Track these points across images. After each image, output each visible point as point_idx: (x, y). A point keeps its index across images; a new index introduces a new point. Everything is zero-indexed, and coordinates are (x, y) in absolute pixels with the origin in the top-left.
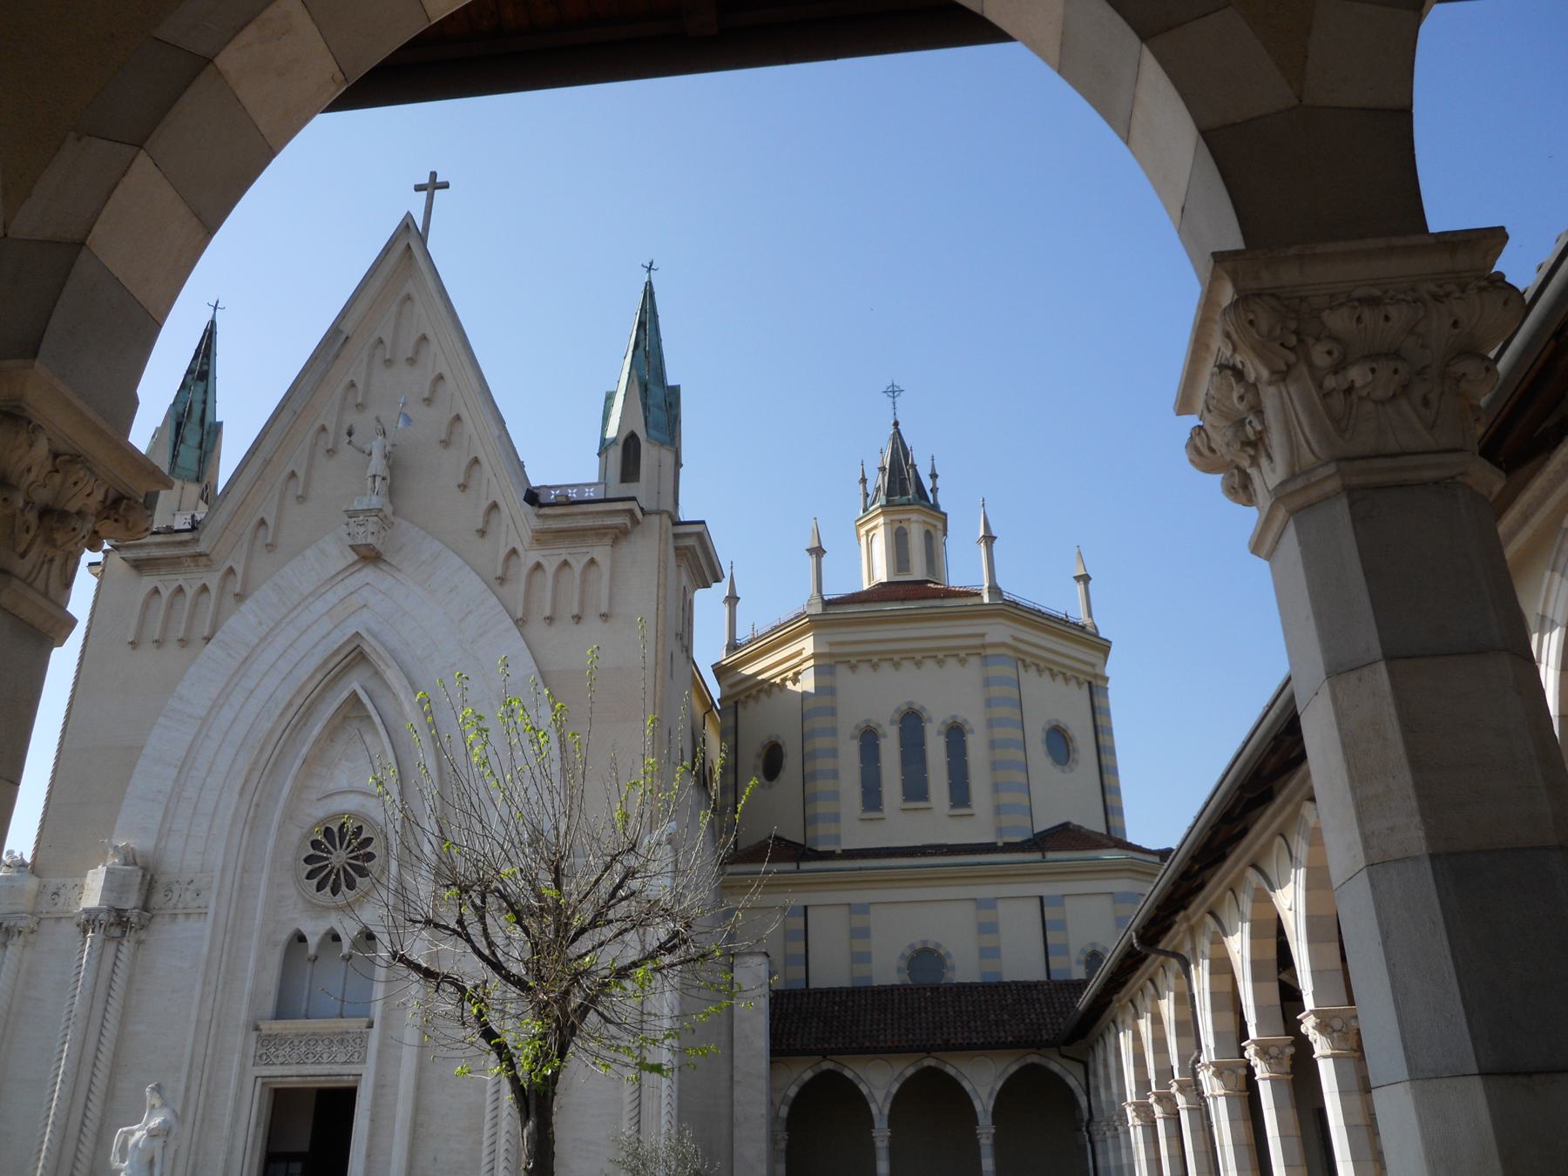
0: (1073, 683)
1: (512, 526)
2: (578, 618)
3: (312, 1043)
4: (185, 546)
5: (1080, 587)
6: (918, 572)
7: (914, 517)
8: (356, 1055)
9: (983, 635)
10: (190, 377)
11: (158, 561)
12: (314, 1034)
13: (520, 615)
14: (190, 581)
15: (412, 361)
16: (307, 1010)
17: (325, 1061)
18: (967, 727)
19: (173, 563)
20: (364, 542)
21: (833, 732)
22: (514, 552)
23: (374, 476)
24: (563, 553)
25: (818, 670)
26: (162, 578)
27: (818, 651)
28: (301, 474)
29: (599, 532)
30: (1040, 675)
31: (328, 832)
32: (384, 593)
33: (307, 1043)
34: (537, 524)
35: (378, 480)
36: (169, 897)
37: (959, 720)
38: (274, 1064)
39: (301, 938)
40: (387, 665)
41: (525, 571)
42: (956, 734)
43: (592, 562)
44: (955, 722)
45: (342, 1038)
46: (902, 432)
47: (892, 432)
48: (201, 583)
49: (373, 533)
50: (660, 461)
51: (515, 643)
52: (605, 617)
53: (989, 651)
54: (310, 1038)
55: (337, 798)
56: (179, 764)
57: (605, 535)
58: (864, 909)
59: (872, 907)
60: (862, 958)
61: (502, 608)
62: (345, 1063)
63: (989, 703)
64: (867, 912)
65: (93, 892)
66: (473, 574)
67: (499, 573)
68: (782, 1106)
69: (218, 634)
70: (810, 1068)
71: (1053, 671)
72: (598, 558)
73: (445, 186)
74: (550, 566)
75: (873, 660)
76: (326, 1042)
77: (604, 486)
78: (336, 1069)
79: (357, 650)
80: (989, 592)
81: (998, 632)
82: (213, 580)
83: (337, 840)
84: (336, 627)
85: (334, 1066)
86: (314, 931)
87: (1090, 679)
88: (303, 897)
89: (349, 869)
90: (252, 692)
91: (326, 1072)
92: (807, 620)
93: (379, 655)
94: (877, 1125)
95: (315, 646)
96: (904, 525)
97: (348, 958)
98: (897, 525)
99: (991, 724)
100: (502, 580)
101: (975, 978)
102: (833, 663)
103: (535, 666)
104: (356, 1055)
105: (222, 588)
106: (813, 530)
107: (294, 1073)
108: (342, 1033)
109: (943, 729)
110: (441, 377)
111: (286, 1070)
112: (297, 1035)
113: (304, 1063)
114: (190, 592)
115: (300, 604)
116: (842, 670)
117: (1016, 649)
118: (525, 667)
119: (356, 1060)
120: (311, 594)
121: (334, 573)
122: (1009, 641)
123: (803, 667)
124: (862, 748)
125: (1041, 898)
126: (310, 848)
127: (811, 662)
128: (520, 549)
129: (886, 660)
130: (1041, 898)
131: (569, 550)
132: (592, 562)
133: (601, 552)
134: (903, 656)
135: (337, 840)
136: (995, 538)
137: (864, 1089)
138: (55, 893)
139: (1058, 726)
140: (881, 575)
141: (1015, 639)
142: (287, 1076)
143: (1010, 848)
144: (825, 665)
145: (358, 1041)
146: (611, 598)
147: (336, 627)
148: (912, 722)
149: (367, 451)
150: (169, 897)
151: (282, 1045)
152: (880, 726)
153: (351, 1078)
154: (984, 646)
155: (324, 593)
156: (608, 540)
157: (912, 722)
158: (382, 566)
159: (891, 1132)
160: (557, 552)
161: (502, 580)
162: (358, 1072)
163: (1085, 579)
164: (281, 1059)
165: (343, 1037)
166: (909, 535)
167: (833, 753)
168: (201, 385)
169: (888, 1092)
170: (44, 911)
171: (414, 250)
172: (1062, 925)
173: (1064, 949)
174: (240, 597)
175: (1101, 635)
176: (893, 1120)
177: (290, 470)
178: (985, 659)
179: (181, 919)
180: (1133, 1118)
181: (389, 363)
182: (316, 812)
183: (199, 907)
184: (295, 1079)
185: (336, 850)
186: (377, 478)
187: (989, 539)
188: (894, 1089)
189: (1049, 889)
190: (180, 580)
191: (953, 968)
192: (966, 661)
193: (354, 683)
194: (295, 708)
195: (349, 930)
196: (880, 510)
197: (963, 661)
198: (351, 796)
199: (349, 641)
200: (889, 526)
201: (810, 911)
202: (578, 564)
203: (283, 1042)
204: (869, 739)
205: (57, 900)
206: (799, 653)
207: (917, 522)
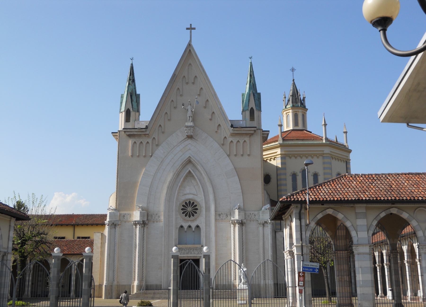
0: (343, 162)
1: (224, 131)
2: (242, 155)
3: (189, 250)
5: (345, 135)
6: (300, 127)
7: (300, 110)
8: (200, 252)
9: (323, 151)
10: (130, 81)
12: (190, 248)
13: (228, 154)
14: (144, 140)
15: (193, 83)
16: (186, 242)
17: (193, 253)
18: (319, 174)
19: (139, 136)
20: (190, 134)
21: (285, 174)
22: (225, 137)
23: (190, 116)
25: (282, 158)
26: (136, 139)
27: (282, 153)
28: (169, 113)
29: (247, 134)
30: (336, 161)
32: (194, 146)
33: (188, 250)
34: (232, 132)
35: (191, 117)
37: (317, 172)
39: (182, 227)
40: (198, 165)
41: (229, 142)
43: (245, 141)
44: (315, 173)
45: (196, 249)
46: (295, 82)
47: (292, 83)
48: (147, 141)
49: (192, 132)
50: (259, 115)
51: (228, 160)
52: (249, 155)
53: (325, 155)
55: (187, 195)
56: (149, 187)
57: (248, 135)
61: (224, 152)
62: (197, 254)
63: (324, 168)
65: (136, 216)
66: (216, 143)
67: (222, 143)
69: (154, 155)
71: (339, 159)
72: (247, 141)
73: (194, 29)
74: (235, 142)
75: (296, 156)
77: (245, 121)
78: (195, 255)
79: (189, 160)
80: (325, 139)
81: (327, 150)
82: (150, 141)
83: (191, 205)
84: (183, 154)
85: (195, 255)
86: (185, 225)
87: (346, 160)
88: (182, 218)
89: (192, 211)
90: (164, 169)
91: (193, 256)
92: (279, 145)
93: (195, 162)
95: (179, 159)
96: (297, 112)
97: (194, 232)
98: (295, 112)
99: (325, 174)
100: (223, 145)
103: (231, 164)
104: (200, 252)
105: (152, 143)
106: (279, 119)
107: (186, 256)
108: (196, 248)
110: (202, 88)
111: (184, 255)
112: (186, 248)
113: (188, 254)
114: (144, 143)
115: (173, 148)
116: (287, 158)
117: (331, 155)
118: (231, 167)
120: (176, 146)
121: (181, 140)
122: (330, 153)
123: (277, 156)
124: (292, 178)
126: (182, 207)
127: (280, 156)
128: (227, 137)
131: (239, 138)
132: (245, 141)
133: (247, 139)
134: (303, 155)
135: (191, 205)
136: (327, 124)
138: (123, 216)
139: (339, 173)
140: (291, 128)
141: (331, 152)
142: (184, 257)
144: (283, 157)
145: (200, 249)
146: (250, 151)
147: (183, 154)
149: (187, 109)
153: (199, 257)
154: (323, 154)
155: (179, 145)
158: (193, 139)
160: (236, 138)
161: (223, 145)
162: (200, 256)
163: (346, 132)
164: (183, 253)
166: (298, 116)
167: (285, 179)
168: (134, 83)
170: (122, 220)
171: (192, 52)
174: (157, 145)
175: (349, 148)
178: (324, 157)
179: (155, 222)
180: (286, 257)
181: (187, 83)
182: (183, 198)
184: (186, 257)
185: (190, 207)
186: (190, 117)
187: (325, 125)
190: (141, 140)
193: (189, 168)
194: (176, 174)
195: (193, 225)
196: (291, 108)
197: (318, 157)
198: (190, 195)
199: (188, 158)
200: (293, 113)
202: (242, 142)
203: (183, 249)
204: (294, 176)
205: (124, 218)
206: (276, 153)
207: (301, 112)
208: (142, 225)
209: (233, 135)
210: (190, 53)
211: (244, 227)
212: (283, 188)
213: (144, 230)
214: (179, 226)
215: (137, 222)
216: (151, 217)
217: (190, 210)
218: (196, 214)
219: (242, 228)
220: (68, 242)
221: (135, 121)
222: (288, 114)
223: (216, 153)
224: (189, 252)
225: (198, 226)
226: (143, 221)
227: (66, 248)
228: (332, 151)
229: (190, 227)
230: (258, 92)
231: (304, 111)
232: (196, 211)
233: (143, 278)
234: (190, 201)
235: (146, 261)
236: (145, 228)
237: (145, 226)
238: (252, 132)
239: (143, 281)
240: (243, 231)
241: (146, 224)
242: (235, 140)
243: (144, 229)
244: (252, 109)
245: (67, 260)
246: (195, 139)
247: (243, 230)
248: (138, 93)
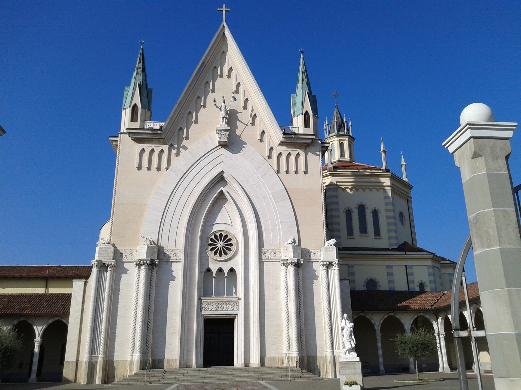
4: (156, 135)
11: (144, 139)
21: (338, 210)
24: (289, 150)
31: (221, 235)
36: (165, 256)
38: (207, 311)
42: (375, 213)
54: (219, 302)
57: (303, 145)
58: (352, 266)
59: (413, 266)
60: (391, 282)
64: (412, 268)
70: (45, 323)
76: (225, 304)
89: (222, 249)
94: (377, 332)
96: (343, 141)
99: (387, 211)
101: (387, 289)
102: (337, 188)
104: (235, 308)
109: (372, 211)
119: (235, 310)
125: (406, 266)
129: (361, 188)
130: (406, 266)
137: (373, 322)
143: (393, 250)
148: (362, 208)
150: (165, 256)
151: (210, 305)
152: (352, 209)
156: (303, 147)
159: (382, 334)
164: (210, 309)
165: (230, 302)
167: (338, 217)
169: (380, 323)
170: (118, 259)
172: (412, 274)
173: (413, 282)
176: (382, 331)
177: (189, 111)
183: (177, 259)
188: (382, 321)
189: (408, 263)
190: (153, 146)
191: (380, 286)
192: (372, 190)
195: (226, 267)
204: (349, 213)
205: (122, 256)
208: (149, 266)
209: (282, 144)
210: (224, 37)
211: (300, 270)
212: (335, 227)
213: (152, 274)
214: (205, 269)
215: (141, 262)
216: (164, 255)
217: (221, 245)
218: (230, 252)
219: (298, 272)
220: (33, 297)
221: (144, 122)
222: (332, 144)
223: (259, 167)
224: (219, 308)
225: (232, 270)
226: (152, 261)
227: (28, 306)
228: (395, 184)
229: (220, 270)
230: (313, 94)
231: (352, 141)
232: (231, 247)
233: (148, 348)
234: (222, 233)
235: (154, 321)
236: (154, 271)
237: (154, 268)
238: (309, 142)
239: (147, 353)
240: (299, 276)
241: (156, 265)
242: (285, 151)
243: (151, 273)
244: (307, 112)
245: (30, 323)
246: (228, 147)
247: (299, 274)
248: (149, 87)
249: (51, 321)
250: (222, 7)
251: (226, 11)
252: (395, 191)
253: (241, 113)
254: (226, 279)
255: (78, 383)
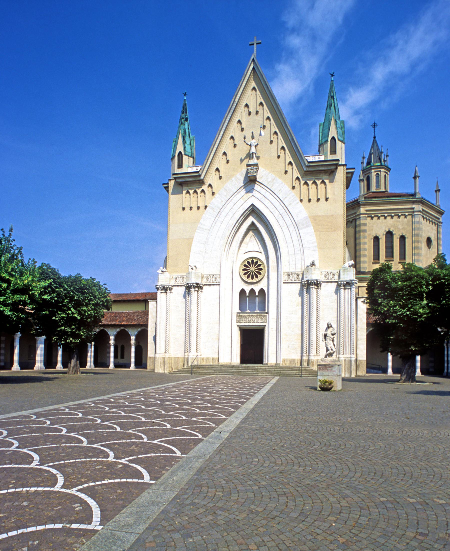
42: (403, 238)
53: (415, 213)
57: (327, 172)
68: (153, 355)
86: (247, 289)
148: (389, 234)
157: (389, 234)
195: (257, 289)
201: (218, 286)
204: (376, 239)
229: (252, 291)
249: (139, 329)
250: (253, 40)
251: (257, 44)
252: (425, 216)
253: (252, 133)
254: (248, 298)
255: (267, 364)
